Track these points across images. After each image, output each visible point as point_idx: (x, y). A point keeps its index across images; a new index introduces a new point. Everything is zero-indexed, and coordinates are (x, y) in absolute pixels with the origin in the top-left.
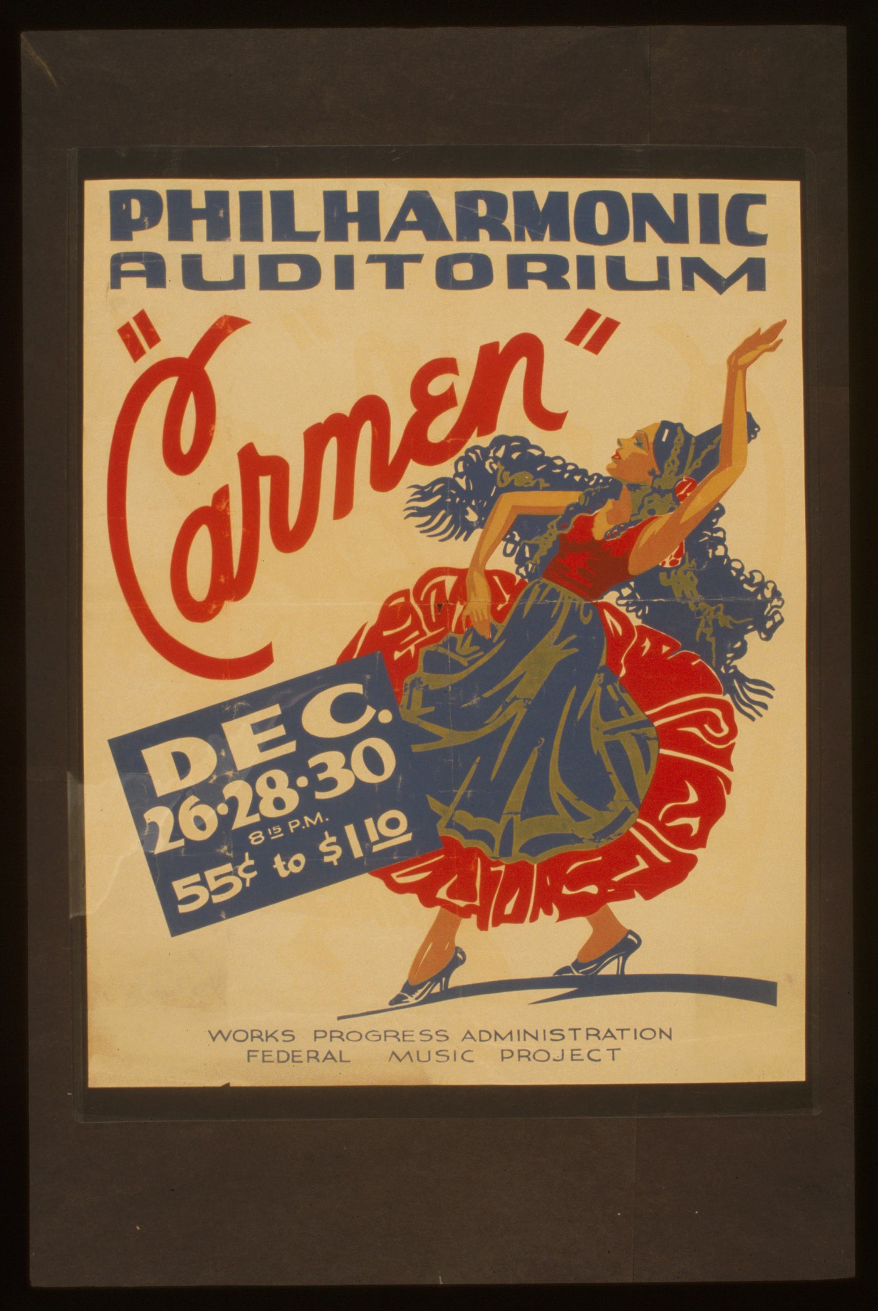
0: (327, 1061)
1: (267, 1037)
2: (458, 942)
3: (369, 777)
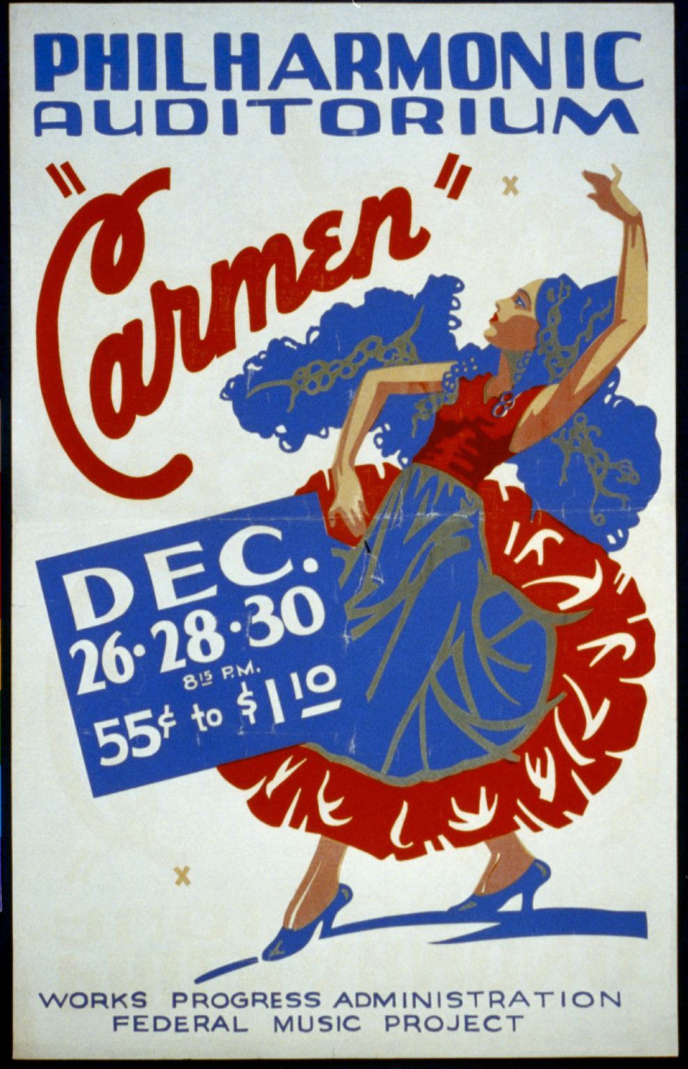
0: (217, 1029)
1: (114, 1001)
2: (343, 878)
3: (298, 629)
